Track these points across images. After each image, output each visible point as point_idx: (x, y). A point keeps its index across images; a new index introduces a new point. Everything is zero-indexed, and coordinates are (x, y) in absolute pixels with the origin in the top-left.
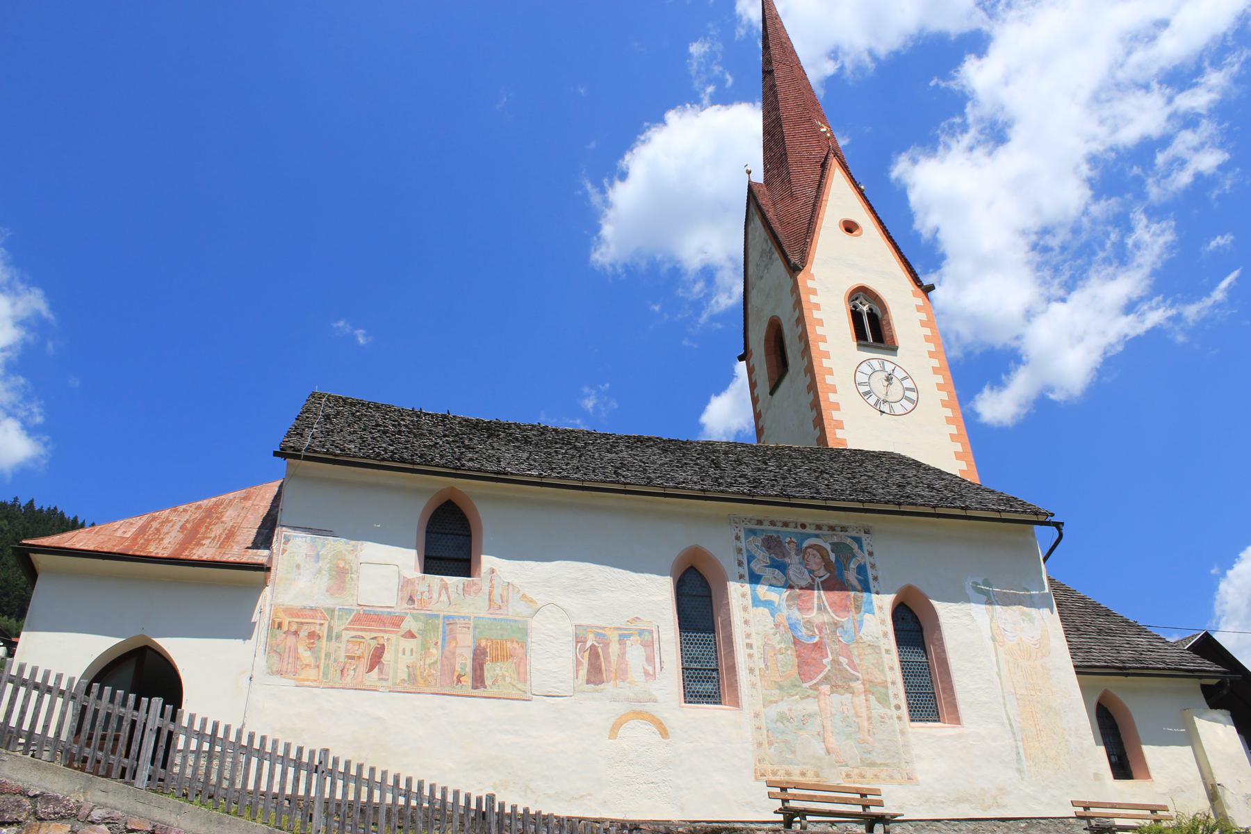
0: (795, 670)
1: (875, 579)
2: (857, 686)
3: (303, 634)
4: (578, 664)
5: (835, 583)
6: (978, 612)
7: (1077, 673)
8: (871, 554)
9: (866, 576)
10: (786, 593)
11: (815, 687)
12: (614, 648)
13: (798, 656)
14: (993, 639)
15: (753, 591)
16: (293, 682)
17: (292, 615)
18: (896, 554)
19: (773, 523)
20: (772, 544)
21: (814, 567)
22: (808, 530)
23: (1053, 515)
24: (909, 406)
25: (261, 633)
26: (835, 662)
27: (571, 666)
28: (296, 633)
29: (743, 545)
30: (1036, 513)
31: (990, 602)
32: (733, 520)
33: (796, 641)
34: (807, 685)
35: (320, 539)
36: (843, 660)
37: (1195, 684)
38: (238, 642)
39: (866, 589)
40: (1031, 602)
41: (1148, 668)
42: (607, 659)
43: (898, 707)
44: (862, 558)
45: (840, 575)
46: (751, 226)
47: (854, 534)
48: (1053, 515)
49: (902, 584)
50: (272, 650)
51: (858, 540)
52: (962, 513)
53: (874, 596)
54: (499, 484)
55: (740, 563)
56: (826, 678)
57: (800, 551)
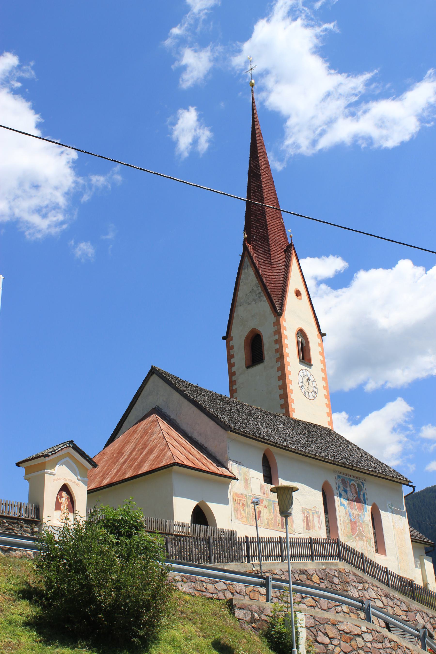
0: (351, 531)
1: (367, 499)
2: (364, 538)
3: (241, 504)
4: (304, 522)
5: (358, 500)
6: (390, 514)
7: (412, 541)
8: (366, 489)
9: (365, 498)
10: (348, 501)
11: (355, 538)
12: (311, 516)
13: (351, 526)
14: (393, 526)
15: (340, 499)
16: (241, 523)
17: (238, 497)
18: (371, 490)
19: (344, 474)
20: (344, 482)
21: (353, 493)
22: (352, 478)
23: (411, 482)
24: (312, 398)
25: (231, 501)
26: (359, 529)
27: (302, 522)
28: (239, 503)
29: (337, 481)
30: (409, 482)
31: (392, 513)
32: (335, 471)
33: (351, 520)
34: (353, 537)
35: (240, 466)
36: (361, 528)
37: (423, 546)
38: (225, 506)
39: (365, 503)
40: (397, 513)
41: (416, 539)
42: (310, 521)
43: (373, 548)
44: (364, 491)
45: (359, 498)
46: (244, 272)
47: (361, 481)
48: (411, 482)
49: (372, 503)
50: (236, 510)
51: (363, 483)
52: (391, 478)
53: (367, 506)
54: (277, 448)
55: (337, 489)
56: (357, 535)
57: (350, 486)
